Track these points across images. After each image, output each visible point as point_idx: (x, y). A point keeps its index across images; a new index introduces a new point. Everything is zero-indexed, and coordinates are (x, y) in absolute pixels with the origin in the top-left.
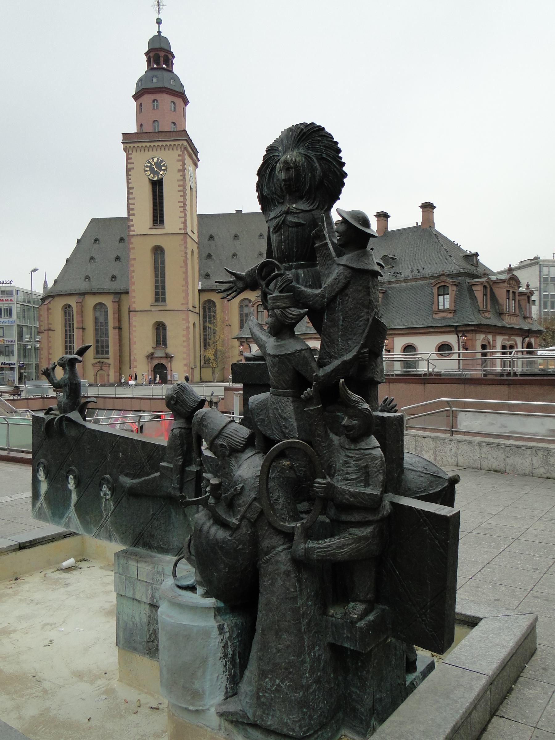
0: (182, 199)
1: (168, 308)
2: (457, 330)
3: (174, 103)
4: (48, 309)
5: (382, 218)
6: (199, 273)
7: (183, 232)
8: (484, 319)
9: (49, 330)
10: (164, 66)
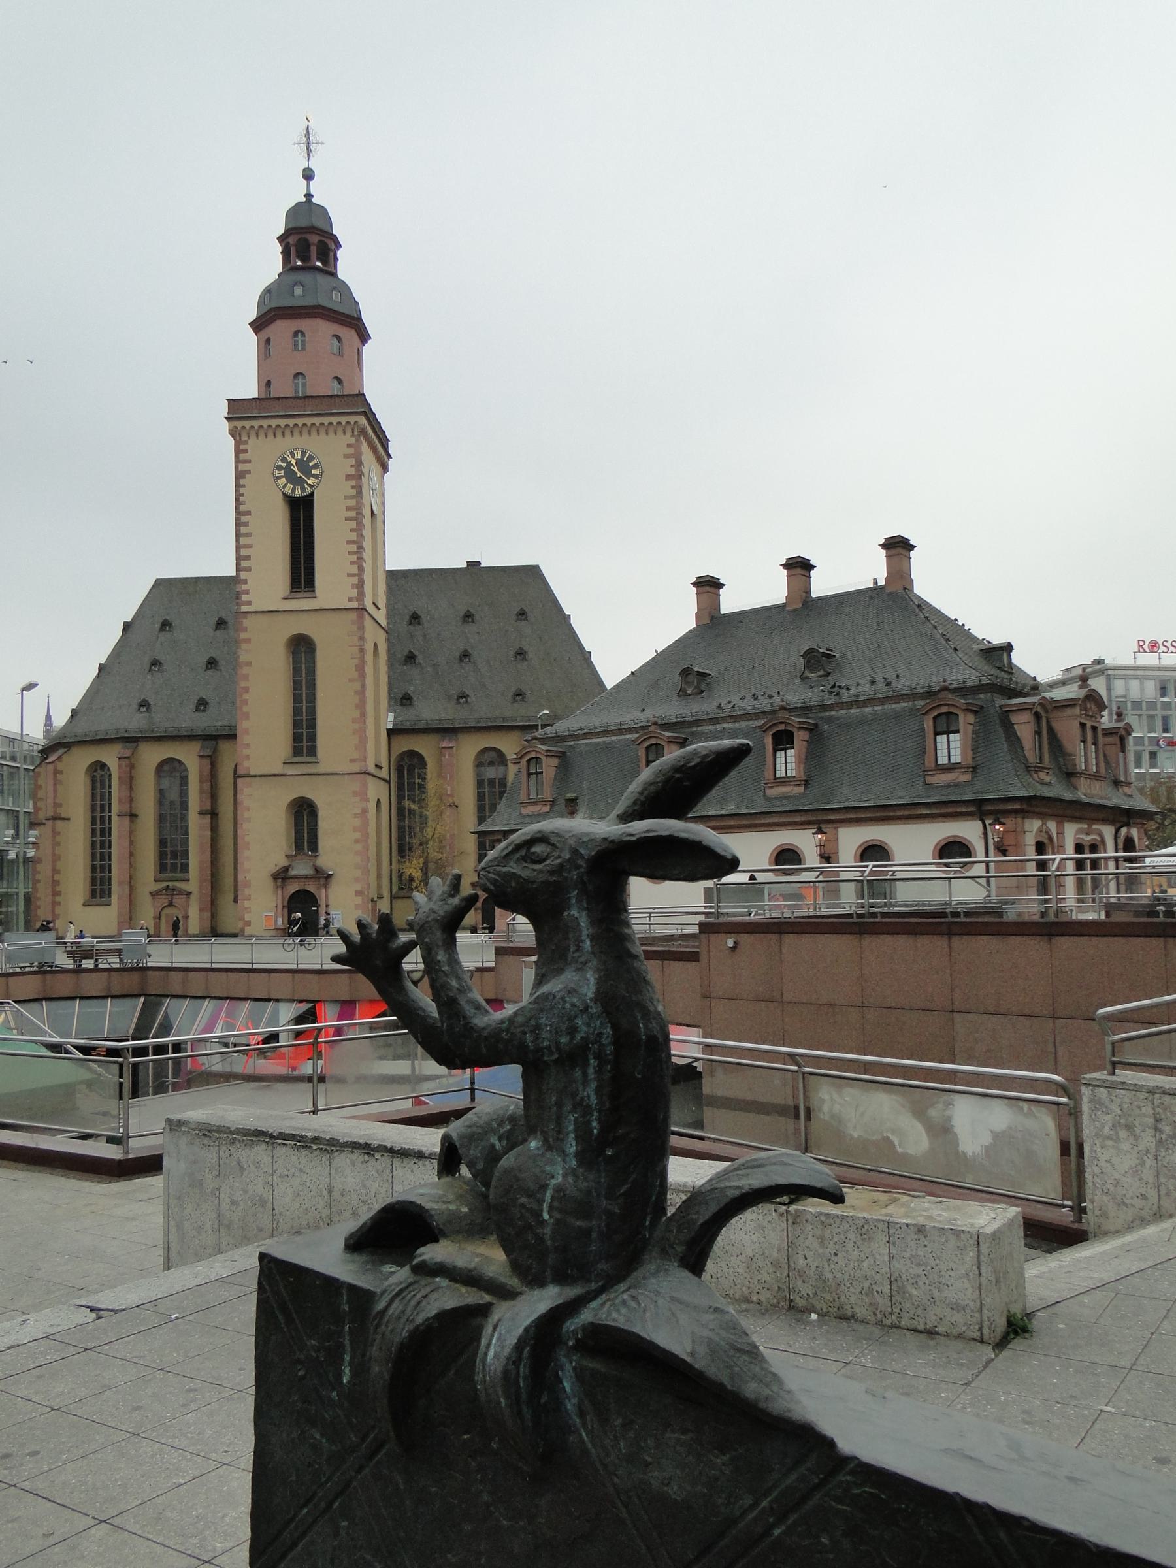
0: (353, 536)
1: (321, 768)
2: (980, 809)
3: (338, 338)
4: (57, 772)
5: (799, 571)
6: (389, 694)
7: (355, 605)
8: (1039, 786)
9: (55, 818)
10: (319, 264)
